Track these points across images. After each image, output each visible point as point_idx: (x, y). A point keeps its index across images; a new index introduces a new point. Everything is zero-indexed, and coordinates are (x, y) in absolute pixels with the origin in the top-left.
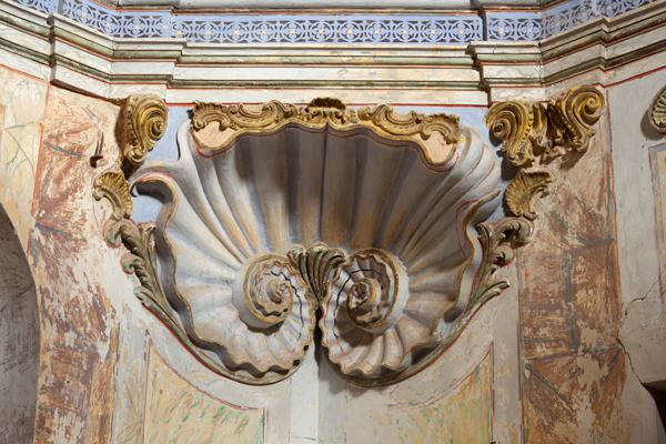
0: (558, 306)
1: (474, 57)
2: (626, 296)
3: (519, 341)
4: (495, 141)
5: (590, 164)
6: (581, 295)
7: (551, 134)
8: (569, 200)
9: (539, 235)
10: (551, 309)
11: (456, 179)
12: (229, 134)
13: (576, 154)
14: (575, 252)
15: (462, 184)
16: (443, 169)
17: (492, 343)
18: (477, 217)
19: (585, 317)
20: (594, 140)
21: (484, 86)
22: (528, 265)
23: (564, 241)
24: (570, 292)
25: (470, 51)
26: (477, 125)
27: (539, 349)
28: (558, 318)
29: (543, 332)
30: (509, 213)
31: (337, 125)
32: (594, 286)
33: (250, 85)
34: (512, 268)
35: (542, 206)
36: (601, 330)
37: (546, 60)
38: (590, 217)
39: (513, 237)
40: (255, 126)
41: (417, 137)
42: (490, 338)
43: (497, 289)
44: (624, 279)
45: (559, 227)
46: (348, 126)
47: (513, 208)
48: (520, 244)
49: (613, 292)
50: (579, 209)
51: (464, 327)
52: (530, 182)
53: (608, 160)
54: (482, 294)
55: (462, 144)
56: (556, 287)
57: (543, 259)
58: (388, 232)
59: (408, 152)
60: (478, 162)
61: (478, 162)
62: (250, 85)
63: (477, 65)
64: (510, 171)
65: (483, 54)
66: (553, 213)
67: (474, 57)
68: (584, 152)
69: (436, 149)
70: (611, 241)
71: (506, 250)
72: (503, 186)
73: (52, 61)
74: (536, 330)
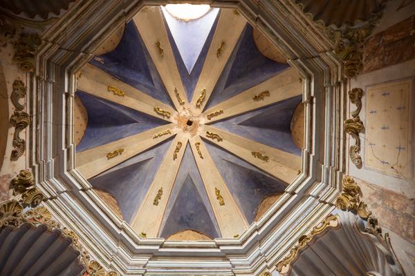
0: (398, 217)
1: (323, 202)
2: (398, 191)
3: (406, 239)
4: (344, 210)
5: (364, 188)
6: (395, 207)
7: (351, 195)
8: (370, 199)
9: (376, 214)
10: (398, 221)
11: (345, 224)
12: (288, 265)
13: (359, 189)
14: (383, 204)
15: (347, 223)
16: (340, 226)
17: (406, 252)
18: (361, 227)
19: (402, 209)
20: (358, 183)
21: (331, 205)
22: (383, 222)
23: (379, 206)
24: (393, 211)
25: (321, 202)
26: (337, 212)
27: (411, 233)
28: (401, 220)
29: (405, 227)
30: (366, 219)
31: (309, 241)
32: (394, 201)
33: (285, 252)
34: (383, 228)
35: (369, 208)
36: (407, 205)
37: (336, 187)
38: (374, 194)
39: (374, 222)
40: (292, 258)
41: (328, 226)
42: (403, 251)
43: (387, 238)
44: (394, 190)
45: (375, 205)
46: (311, 239)
47: (365, 217)
48: (376, 221)
49: (397, 195)
50: (372, 197)
51: (398, 260)
52: (361, 208)
53: (363, 182)
54: (388, 244)
55: (338, 217)
56: (392, 215)
57: (383, 215)
58: (363, 272)
59: (329, 230)
60: (345, 217)
61: (345, 217)
62: (285, 252)
63: (325, 203)
64: (354, 210)
65: (323, 199)
66: (372, 206)
67: (323, 202)
68: (359, 188)
69: (334, 224)
70: (382, 190)
71: (377, 227)
72: (358, 216)
73: (53, 42)
74: (403, 231)
